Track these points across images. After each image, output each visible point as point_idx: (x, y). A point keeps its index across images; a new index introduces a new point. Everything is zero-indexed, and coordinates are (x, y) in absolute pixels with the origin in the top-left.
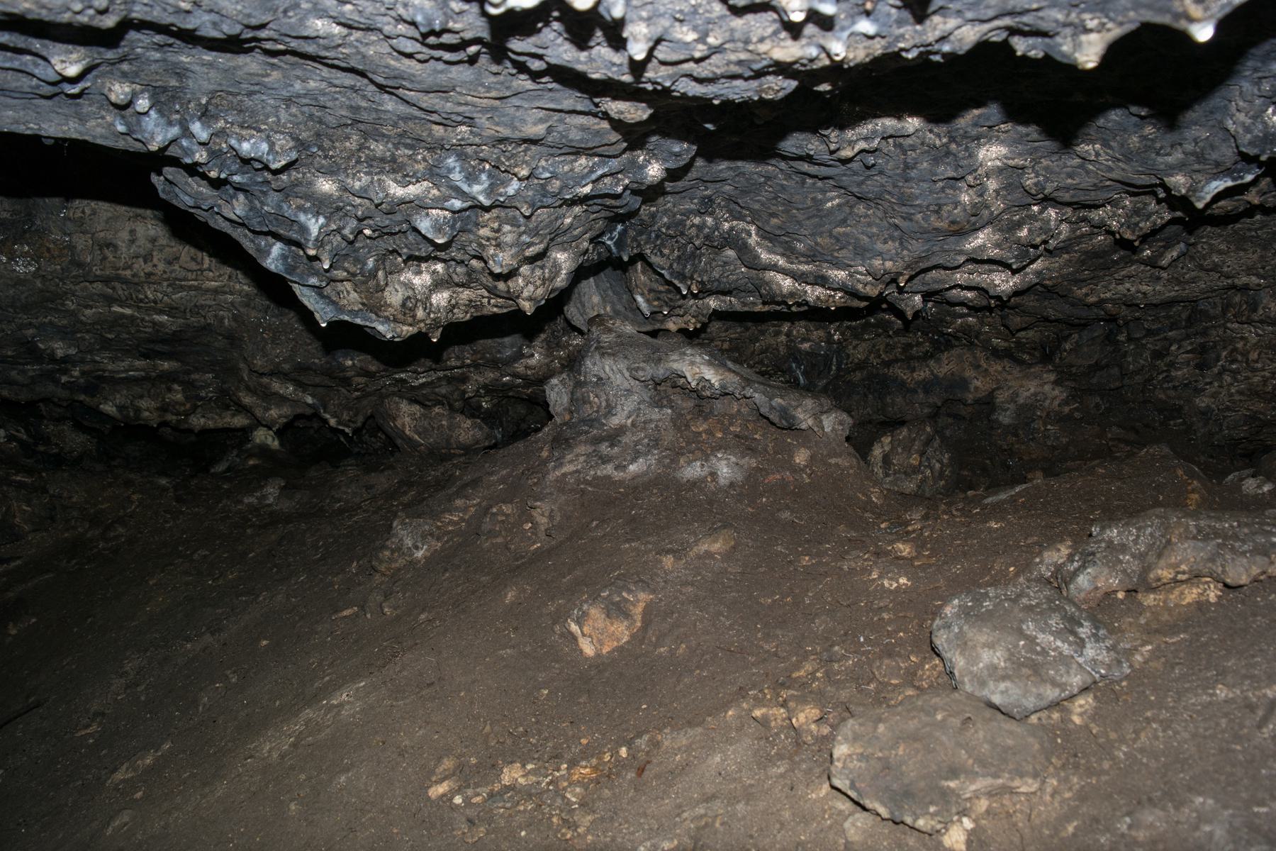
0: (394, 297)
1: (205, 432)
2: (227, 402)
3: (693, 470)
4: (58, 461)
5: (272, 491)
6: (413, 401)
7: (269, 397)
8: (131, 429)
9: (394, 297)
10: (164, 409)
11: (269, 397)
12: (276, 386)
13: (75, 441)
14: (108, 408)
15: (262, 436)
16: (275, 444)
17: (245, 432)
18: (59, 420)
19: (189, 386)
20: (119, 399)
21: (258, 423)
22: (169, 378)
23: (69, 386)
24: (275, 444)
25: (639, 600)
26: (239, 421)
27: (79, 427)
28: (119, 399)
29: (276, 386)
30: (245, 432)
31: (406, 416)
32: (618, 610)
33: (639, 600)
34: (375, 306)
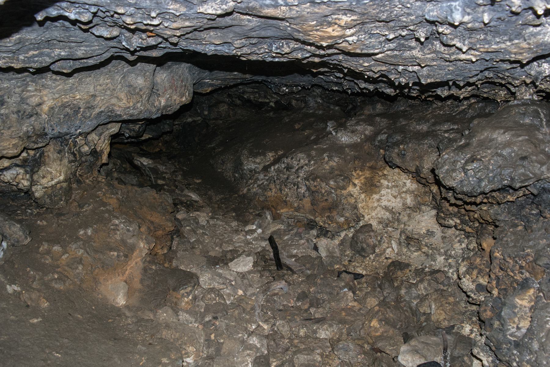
0: (282, 90)
1: (261, 102)
2: (265, 97)
3: (317, 112)
4: (236, 105)
5: (271, 114)
6: (296, 100)
7: (272, 97)
8: (249, 101)
9: (282, 90)
10: (255, 98)
11: (272, 97)
12: (273, 95)
13: (238, 102)
14: (245, 97)
15: (272, 104)
16: (274, 106)
17: (269, 103)
18: (236, 98)
19: (259, 94)
20: (247, 95)
21: (271, 102)
22: (257, 92)
23: (240, 93)
24: (274, 106)
25: (302, 123)
26: (267, 101)
27: (239, 99)
28: (247, 95)
29: (273, 95)
30: (269, 103)
31: (294, 102)
32: (299, 124)
33: (302, 123)
34: (279, 91)
